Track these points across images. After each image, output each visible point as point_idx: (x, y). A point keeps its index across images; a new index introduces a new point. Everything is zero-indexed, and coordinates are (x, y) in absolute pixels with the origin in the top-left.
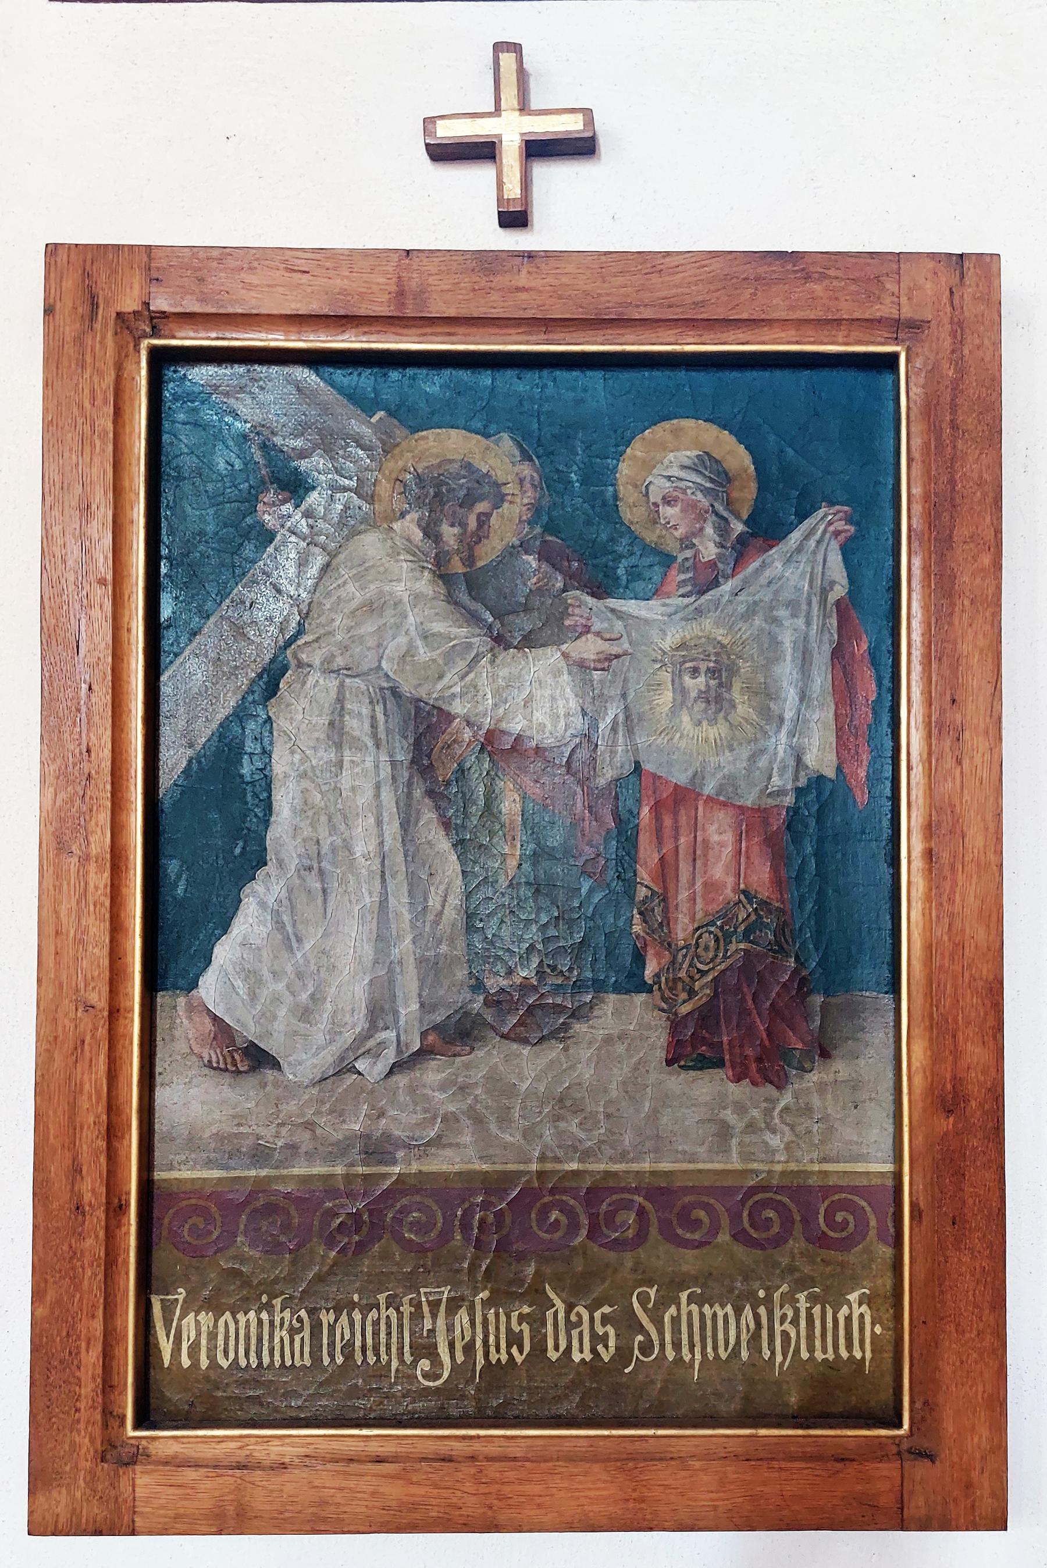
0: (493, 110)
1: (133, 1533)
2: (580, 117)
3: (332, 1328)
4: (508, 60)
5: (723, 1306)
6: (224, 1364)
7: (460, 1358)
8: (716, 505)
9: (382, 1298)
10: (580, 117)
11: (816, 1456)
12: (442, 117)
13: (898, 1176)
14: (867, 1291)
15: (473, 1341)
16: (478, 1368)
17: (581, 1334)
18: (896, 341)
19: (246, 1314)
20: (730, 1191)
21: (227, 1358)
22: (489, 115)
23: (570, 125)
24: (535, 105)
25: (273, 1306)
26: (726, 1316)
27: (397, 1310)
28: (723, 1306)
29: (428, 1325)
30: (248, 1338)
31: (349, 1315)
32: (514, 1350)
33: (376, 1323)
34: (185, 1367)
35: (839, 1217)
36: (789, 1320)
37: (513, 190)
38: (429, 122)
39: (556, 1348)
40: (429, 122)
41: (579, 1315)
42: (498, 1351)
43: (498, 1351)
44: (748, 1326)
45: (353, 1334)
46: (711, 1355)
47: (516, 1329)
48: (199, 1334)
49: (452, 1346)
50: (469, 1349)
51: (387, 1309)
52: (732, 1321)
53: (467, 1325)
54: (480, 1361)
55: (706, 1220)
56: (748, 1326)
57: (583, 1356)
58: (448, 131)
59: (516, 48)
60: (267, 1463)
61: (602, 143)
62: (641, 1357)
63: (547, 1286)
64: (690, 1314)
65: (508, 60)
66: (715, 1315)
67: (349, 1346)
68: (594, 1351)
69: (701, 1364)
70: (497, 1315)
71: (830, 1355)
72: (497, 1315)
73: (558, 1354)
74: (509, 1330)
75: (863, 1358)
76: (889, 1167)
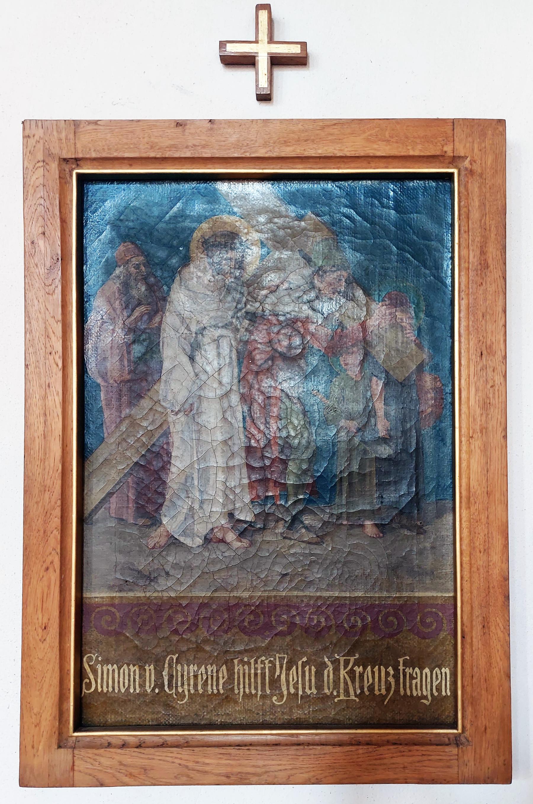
0: (276, 39)
1: (73, 786)
3: (361, 676)
4: (263, 15)
11: (356, 743)
13: (455, 598)
14: (408, 658)
15: (373, 684)
19: (112, 666)
20: (373, 606)
23: (296, 50)
24: (276, 39)
25: (250, 663)
28: (134, 666)
29: (278, 673)
35: (428, 620)
37: (264, 83)
38: (222, 44)
39: (124, 687)
40: (222, 44)
42: (417, 690)
45: (373, 678)
46: (247, 690)
52: (116, 671)
54: (300, 693)
58: (232, 49)
59: (267, 7)
61: (311, 61)
62: (86, 691)
65: (263, 15)
69: (243, 696)
70: (310, 670)
76: (452, 594)
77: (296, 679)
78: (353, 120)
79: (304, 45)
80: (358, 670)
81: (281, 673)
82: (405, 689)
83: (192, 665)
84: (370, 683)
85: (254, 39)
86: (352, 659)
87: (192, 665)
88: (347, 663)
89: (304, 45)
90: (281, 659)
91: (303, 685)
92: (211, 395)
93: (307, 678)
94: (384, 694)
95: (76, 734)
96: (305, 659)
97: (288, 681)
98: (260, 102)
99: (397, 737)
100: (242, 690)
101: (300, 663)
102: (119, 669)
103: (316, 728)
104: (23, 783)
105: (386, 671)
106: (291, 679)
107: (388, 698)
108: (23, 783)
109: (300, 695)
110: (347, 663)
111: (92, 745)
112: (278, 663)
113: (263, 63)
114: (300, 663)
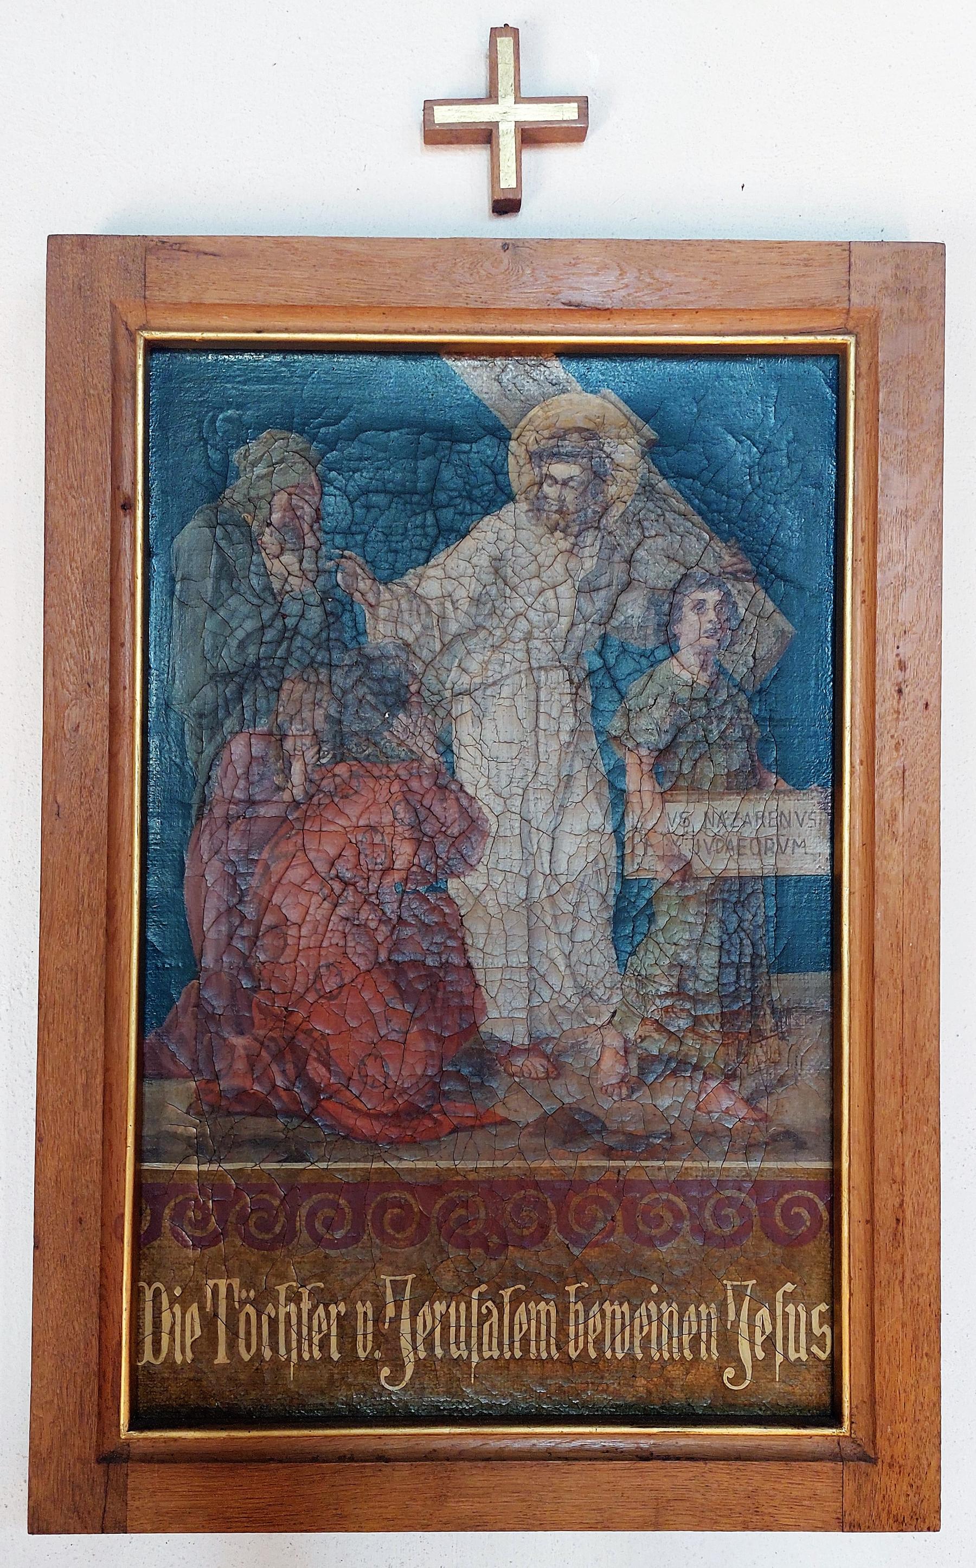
5: (621, 1305)
7: (760, 1355)
15: (699, 1333)
16: (474, 1365)
21: (248, 1350)
22: (517, 88)
23: (570, 112)
27: (298, 1305)
28: (621, 1305)
31: (601, 1304)
33: (273, 1322)
34: (336, 1359)
38: (429, 106)
40: (429, 106)
41: (489, 1311)
44: (594, 1326)
45: (603, 1324)
48: (604, 1328)
50: (525, 1340)
52: (581, 1314)
53: (524, 1320)
58: (443, 115)
59: (514, 33)
67: (525, 1340)
71: (496, 1354)
75: (289, 1360)
77: (769, 1329)
79: (583, 103)
82: (660, 1349)
84: (597, 1333)
90: (398, 1288)
92: (733, 865)
95: (135, 1434)
96: (789, 1287)
97: (414, 1333)
100: (294, 1355)
101: (475, 1295)
103: (632, 1424)
105: (783, 1311)
109: (474, 1365)
112: (389, 1297)
113: (507, 142)
114: (475, 1295)
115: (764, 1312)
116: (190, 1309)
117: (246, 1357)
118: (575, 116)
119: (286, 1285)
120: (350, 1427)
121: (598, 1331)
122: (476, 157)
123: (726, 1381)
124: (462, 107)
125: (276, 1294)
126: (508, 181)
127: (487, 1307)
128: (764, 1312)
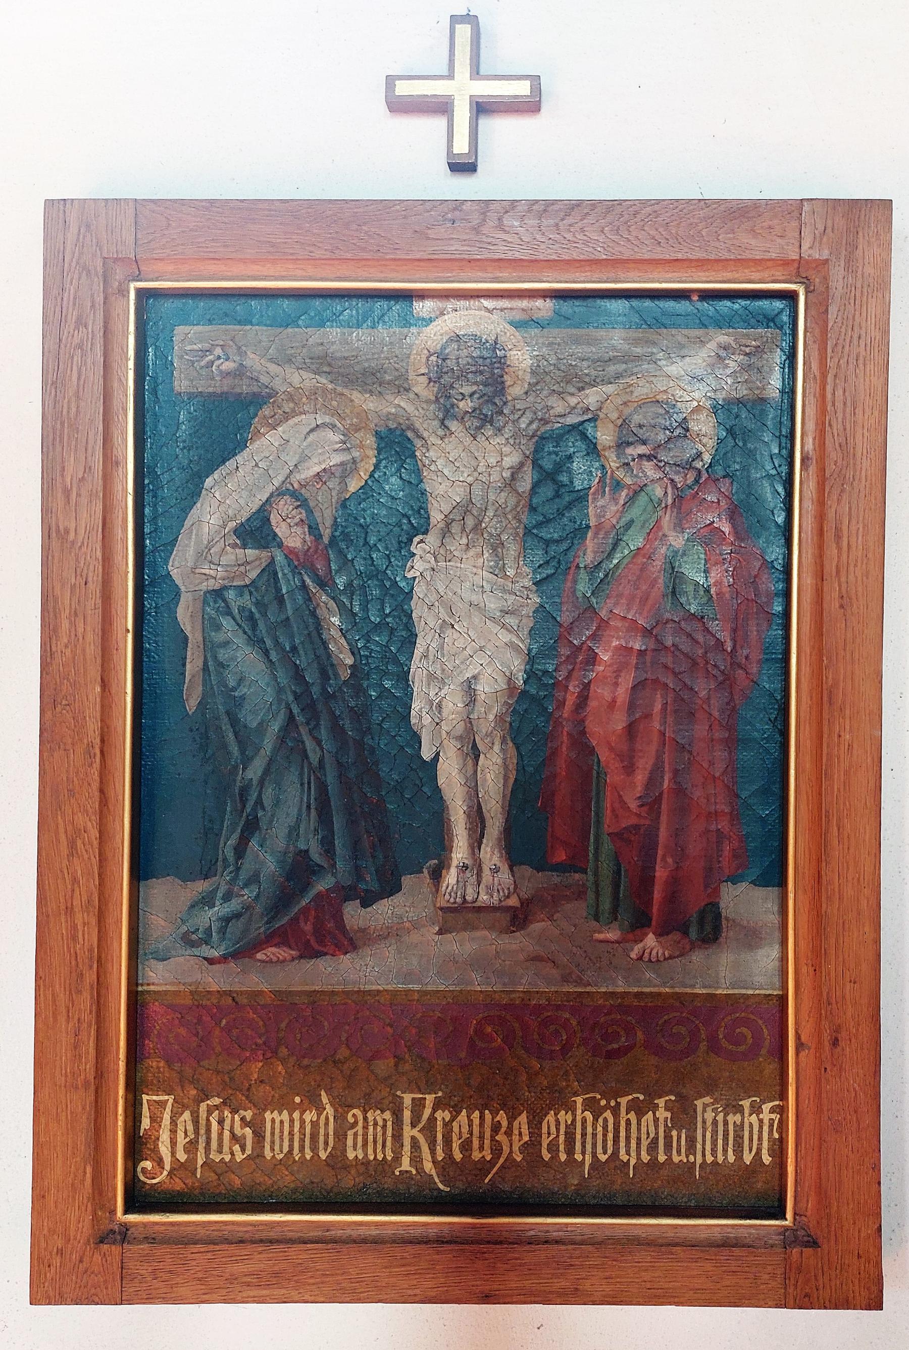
0: (446, 73)
2: (527, 83)
6: (603, 1158)
7: (182, 1157)
8: (560, 425)
9: (746, 1103)
10: (527, 83)
12: (401, 78)
17: (356, 1134)
18: (124, 293)
22: (441, 77)
23: (523, 89)
24: (482, 72)
26: (282, 1122)
30: (291, 1134)
32: (237, 1148)
36: (503, 1130)
37: (461, 146)
38: (391, 81)
43: (355, 1148)
44: (648, 1133)
47: (238, 1131)
48: (471, 1133)
49: (173, 1143)
50: (192, 1147)
51: (750, 1115)
52: (634, 1122)
55: (750, 1041)
56: (648, 1133)
57: (680, 1158)
58: (403, 89)
59: (470, 19)
60: (234, 1241)
63: (323, 1093)
64: (584, 1121)
65: (464, 31)
66: (273, 1121)
68: (687, 1157)
72: (482, 1118)
73: (607, 1156)
74: (234, 1136)
78: (578, 204)
79: (535, 80)
80: (443, 1115)
81: (208, 1120)
83: (563, 1112)
85: (446, 73)
86: (430, 1098)
87: (563, 1112)
88: (418, 1105)
89: (535, 80)
91: (716, 1145)
93: (708, 1135)
94: (488, 1158)
95: (132, 1218)
98: (458, 175)
99: (163, 1228)
102: (596, 1119)
104: (879, 1307)
106: (644, 1136)
107: (498, 1165)
108: (879, 1307)
110: (418, 1105)
111: (152, 1238)
113: (462, 113)
115: (187, 1115)
116: (519, 1119)
117: (603, 1158)
118: (527, 92)
119: (750, 1100)
120: (487, 1217)
121: (652, 1135)
122: (439, 123)
123: (139, 1169)
124: (437, 82)
125: (741, 1108)
126: (461, 146)
127: (354, 1115)
128: (187, 1115)
